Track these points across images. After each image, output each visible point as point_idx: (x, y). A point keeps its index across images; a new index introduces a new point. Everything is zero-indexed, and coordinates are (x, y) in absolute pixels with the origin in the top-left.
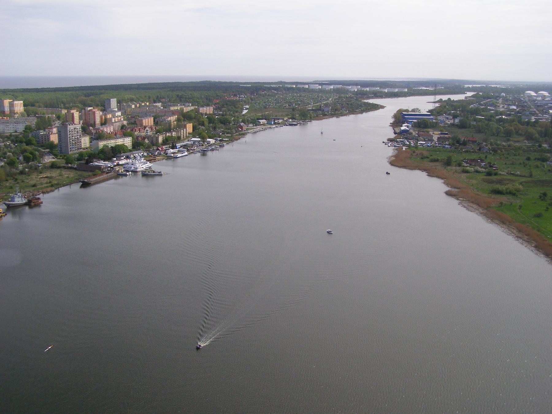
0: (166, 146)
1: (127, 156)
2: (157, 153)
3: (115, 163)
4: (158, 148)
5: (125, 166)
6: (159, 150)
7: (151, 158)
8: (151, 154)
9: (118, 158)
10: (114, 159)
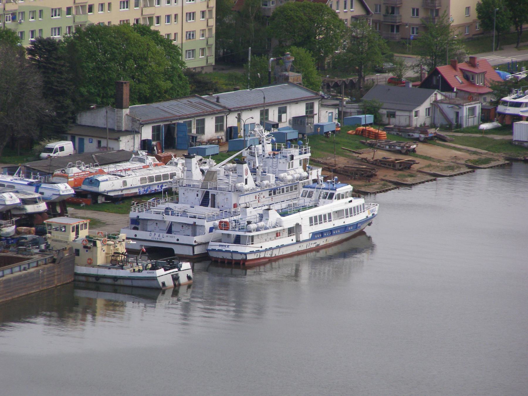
0: (507, 59)
1: (170, 129)
2: (422, 109)
3: (65, 177)
4: (434, 72)
5: (144, 215)
6: (446, 87)
7: (369, 154)
8: (369, 118)
9: (90, 146)
10: (56, 145)
